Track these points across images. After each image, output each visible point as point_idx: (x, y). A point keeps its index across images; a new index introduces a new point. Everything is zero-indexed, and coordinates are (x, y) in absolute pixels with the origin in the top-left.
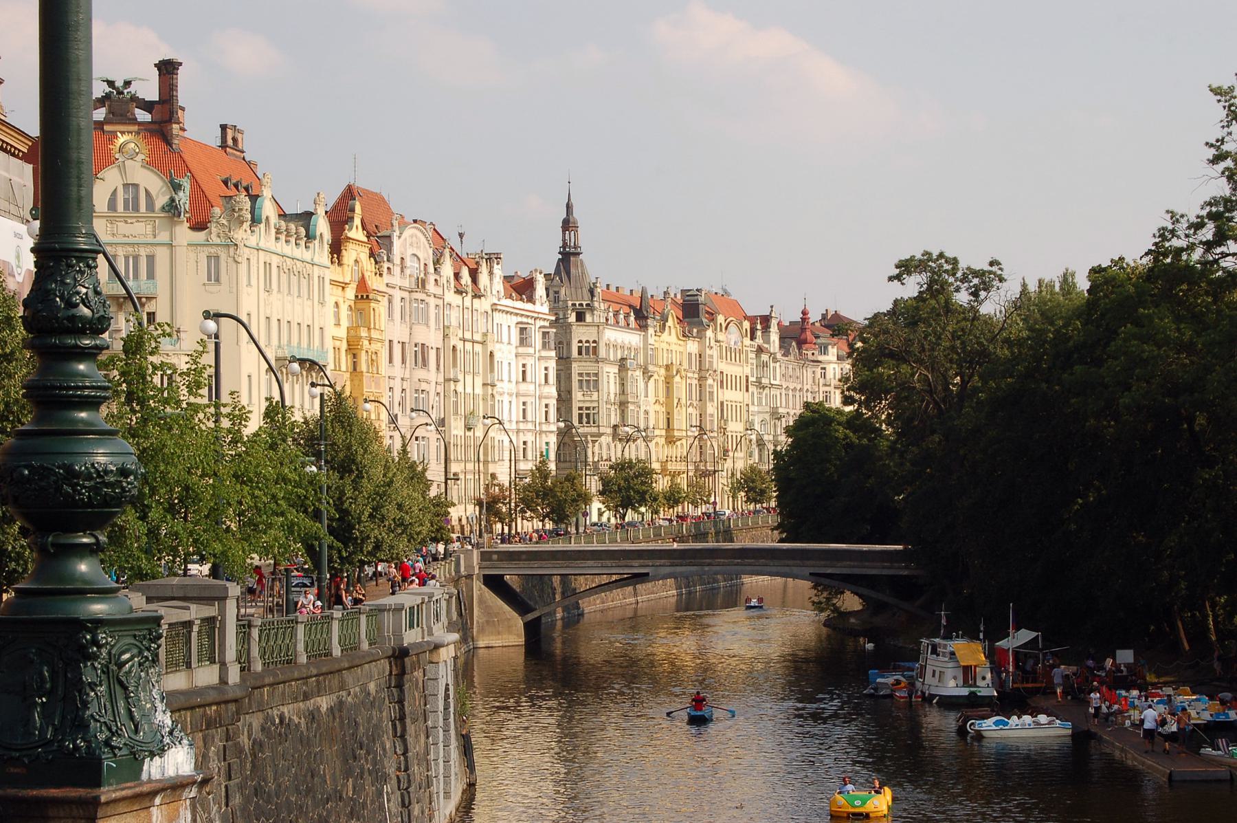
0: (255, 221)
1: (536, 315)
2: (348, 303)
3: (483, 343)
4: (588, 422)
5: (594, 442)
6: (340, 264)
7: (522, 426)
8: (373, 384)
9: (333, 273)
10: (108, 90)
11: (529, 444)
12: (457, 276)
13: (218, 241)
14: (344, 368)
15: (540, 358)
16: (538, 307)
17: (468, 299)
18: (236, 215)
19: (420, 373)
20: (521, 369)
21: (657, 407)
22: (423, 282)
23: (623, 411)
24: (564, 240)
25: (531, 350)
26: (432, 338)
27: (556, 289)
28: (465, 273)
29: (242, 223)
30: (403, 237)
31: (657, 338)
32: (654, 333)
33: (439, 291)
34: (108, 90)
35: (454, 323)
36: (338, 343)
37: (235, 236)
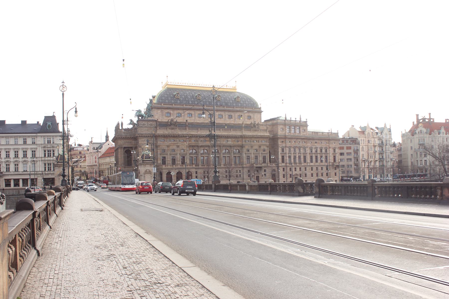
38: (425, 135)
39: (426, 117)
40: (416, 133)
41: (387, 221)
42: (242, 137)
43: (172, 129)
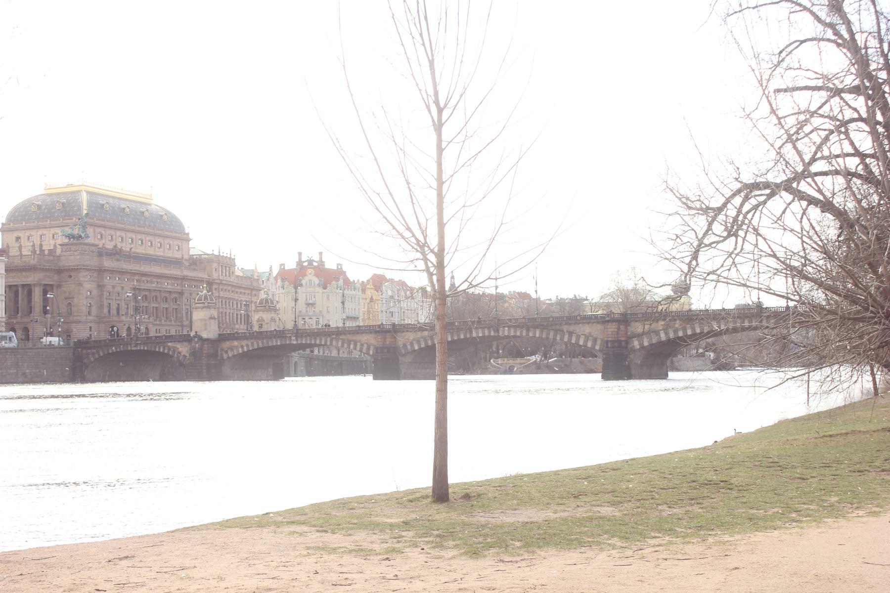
42: (184, 279)
43: (118, 260)
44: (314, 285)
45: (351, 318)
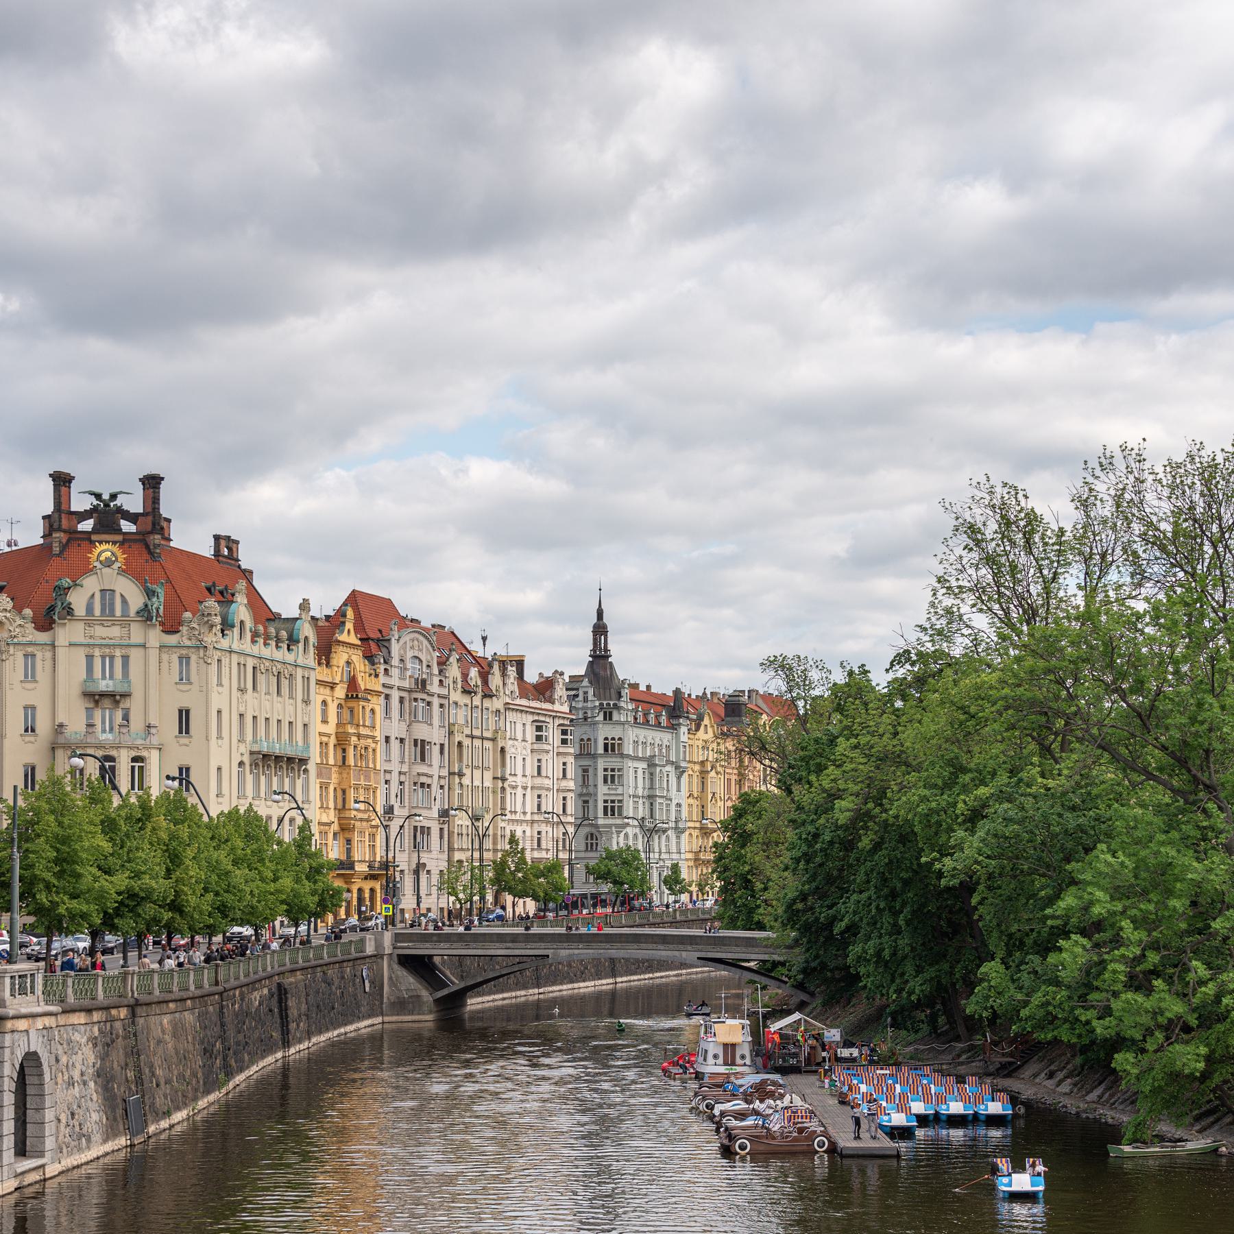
0: (226, 626)
1: (554, 714)
2: (336, 702)
3: (493, 740)
4: (613, 814)
5: (619, 833)
6: (328, 665)
7: (536, 817)
8: (362, 777)
9: (323, 674)
10: (96, 502)
11: (544, 834)
12: (465, 676)
13: (188, 643)
14: (331, 761)
15: (559, 754)
16: (557, 707)
17: (477, 700)
18: (206, 619)
19: (423, 769)
20: (536, 764)
21: (691, 801)
22: (424, 682)
23: (652, 804)
24: (595, 644)
25: (546, 747)
26: (435, 734)
27: (585, 690)
28: (474, 672)
29: (212, 626)
30: (402, 641)
31: (692, 736)
32: (686, 732)
33: (444, 692)
34: (96, 502)
35: (461, 721)
36: (325, 739)
37: (205, 639)
38: (137, 633)
39: (124, 502)
40: (69, 611)
41: (589, 1230)
44: (125, 612)
45: (278, 758)
